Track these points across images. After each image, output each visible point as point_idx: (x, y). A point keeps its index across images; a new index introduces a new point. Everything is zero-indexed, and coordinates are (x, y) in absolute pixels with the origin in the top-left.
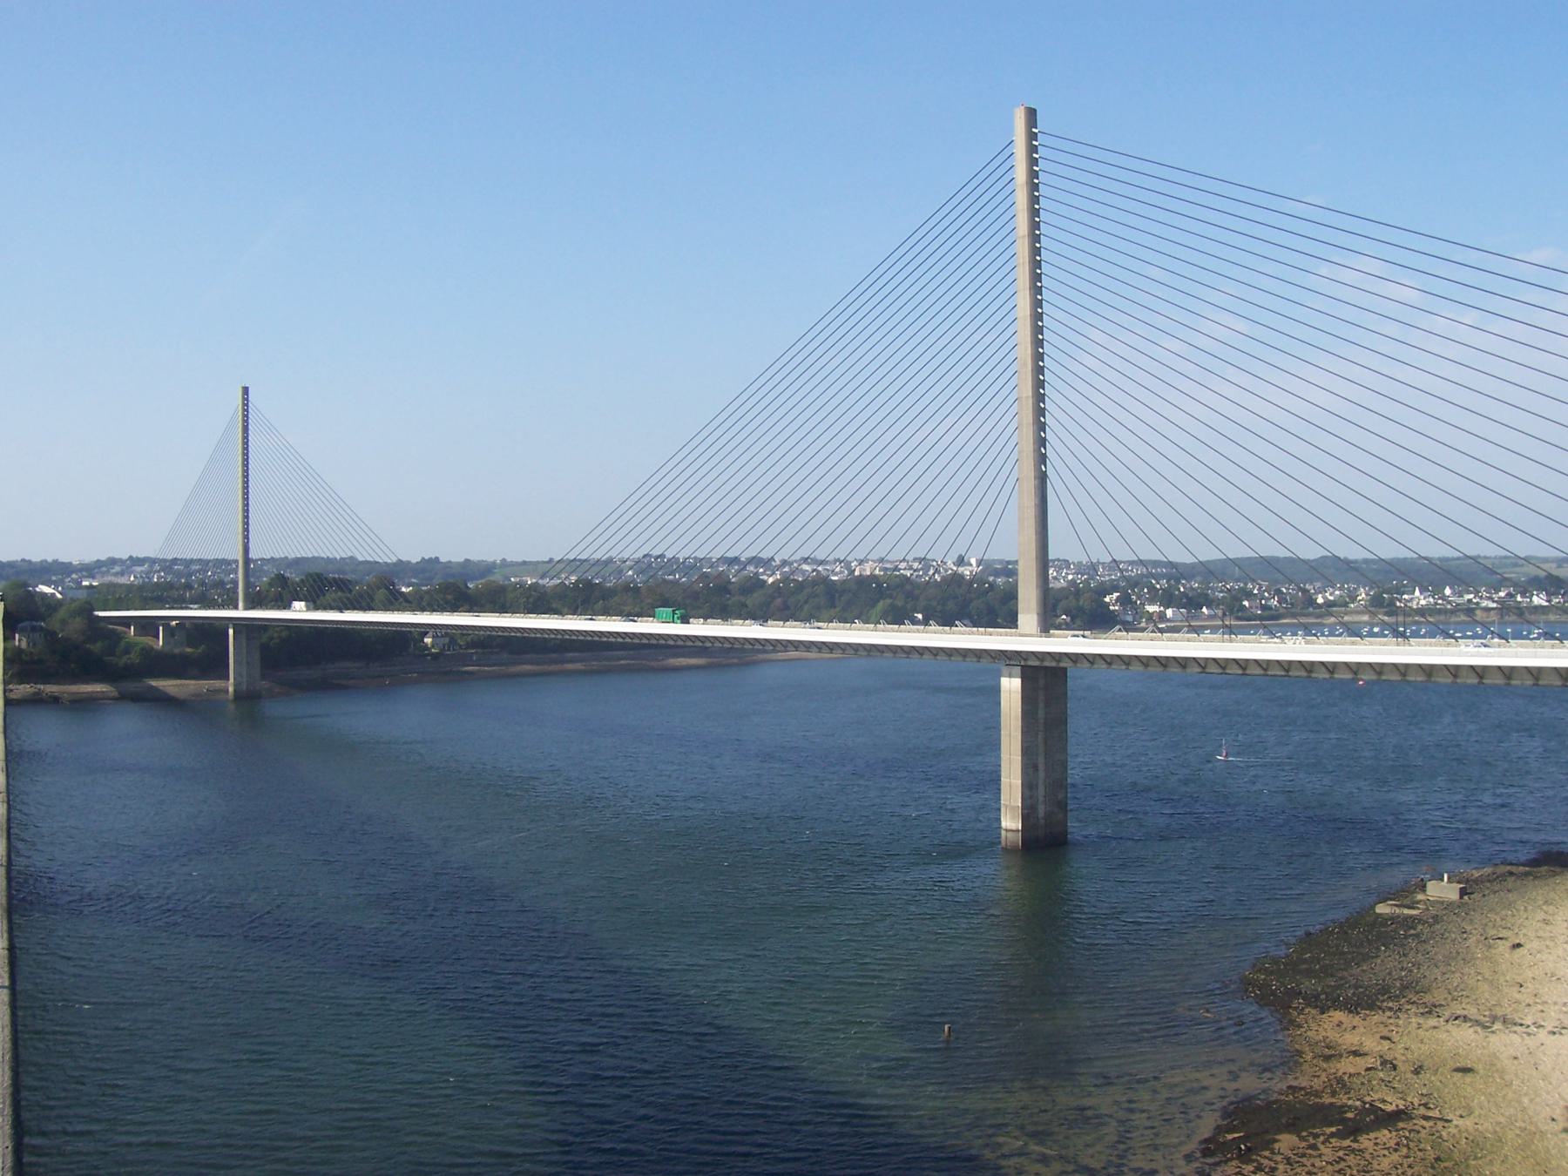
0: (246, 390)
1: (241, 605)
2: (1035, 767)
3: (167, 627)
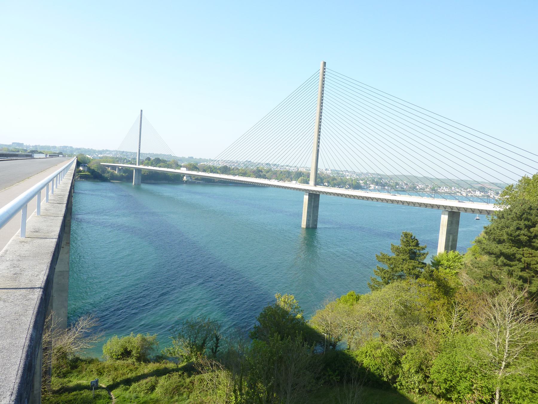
0: (142, 111)
1: (137, 164)
2: (310, 216)
3: (118, 168)
